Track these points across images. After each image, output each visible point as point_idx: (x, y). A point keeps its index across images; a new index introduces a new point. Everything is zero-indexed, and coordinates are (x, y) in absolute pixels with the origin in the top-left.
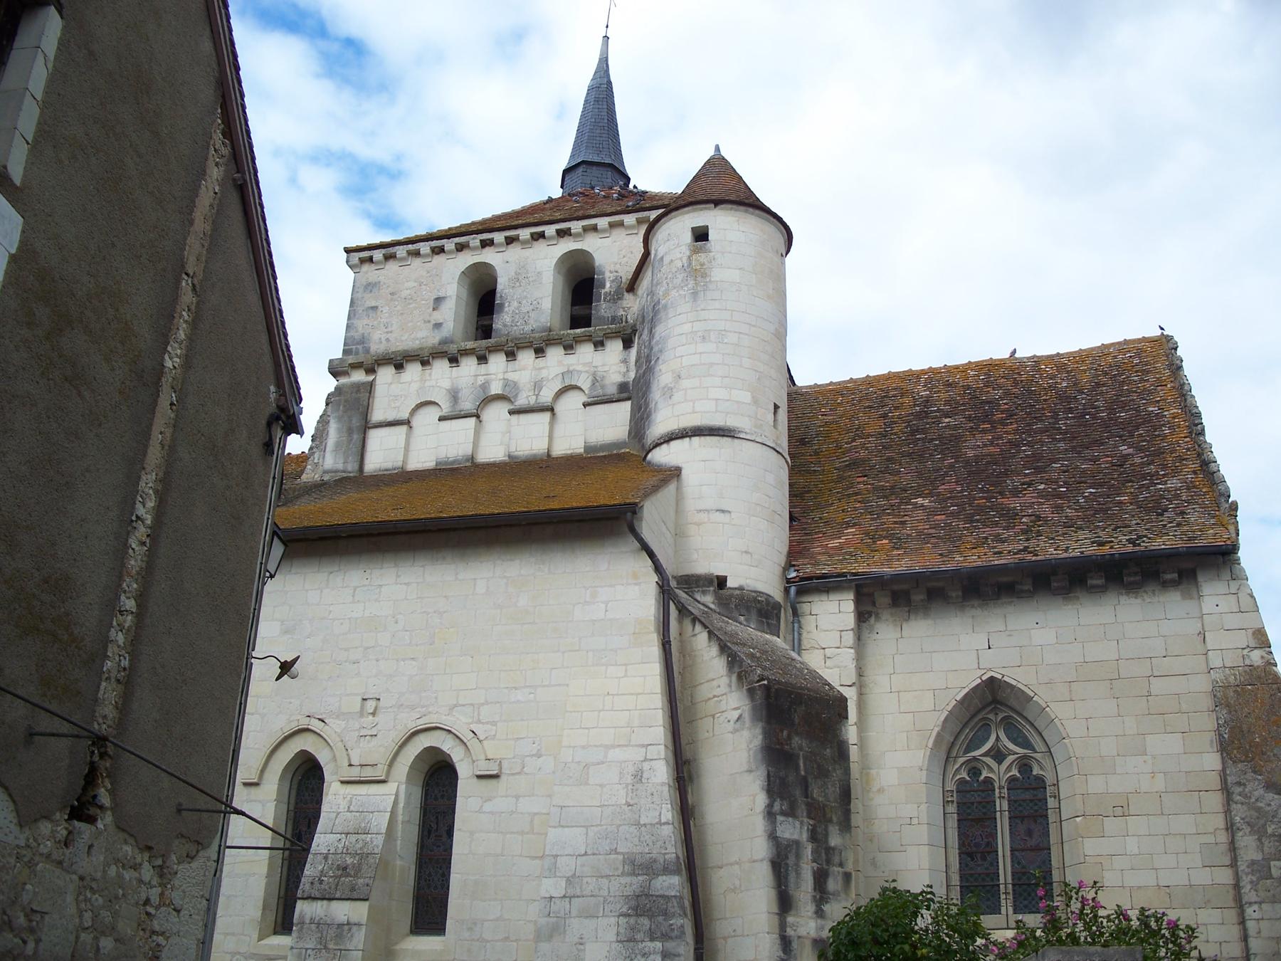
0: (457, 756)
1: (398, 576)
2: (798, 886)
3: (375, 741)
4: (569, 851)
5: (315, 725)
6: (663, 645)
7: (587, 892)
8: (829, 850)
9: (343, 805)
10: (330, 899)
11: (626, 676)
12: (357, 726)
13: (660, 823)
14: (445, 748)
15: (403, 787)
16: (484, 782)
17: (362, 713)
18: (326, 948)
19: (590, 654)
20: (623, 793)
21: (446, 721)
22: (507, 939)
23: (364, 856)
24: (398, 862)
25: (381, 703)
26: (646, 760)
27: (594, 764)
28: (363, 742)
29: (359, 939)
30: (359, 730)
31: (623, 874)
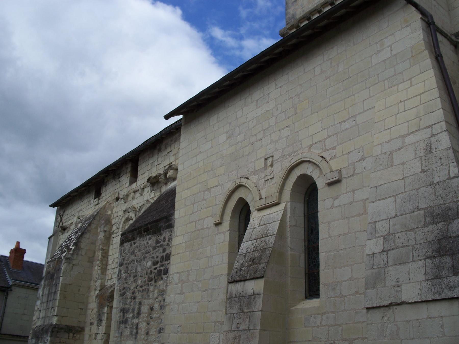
0: (315, 175)
1: (276, 85)
3: (273, 181)
4: (385, 216)
5: (244, 181)
6: (436, 58)
7: (399, 245)
9: (257, 223)
10: (245, 280)
11: (411, 86)
12: (264, 175)
13: (450, 178)
14: (308, 173)
15: (289, 204)
17: (265, 167)
18: (243, 312)
19: (386, 82)
20: (418, 164)
21: (306, 155)
22: (357, 293)
23: (263, 250)
24: (290, 252)
25: (275, 158)
26: (433, 135)
27: (396, 151)
28: (267, 184)
29: (259, 302)
30: (264, 178)
31: (425, 225)
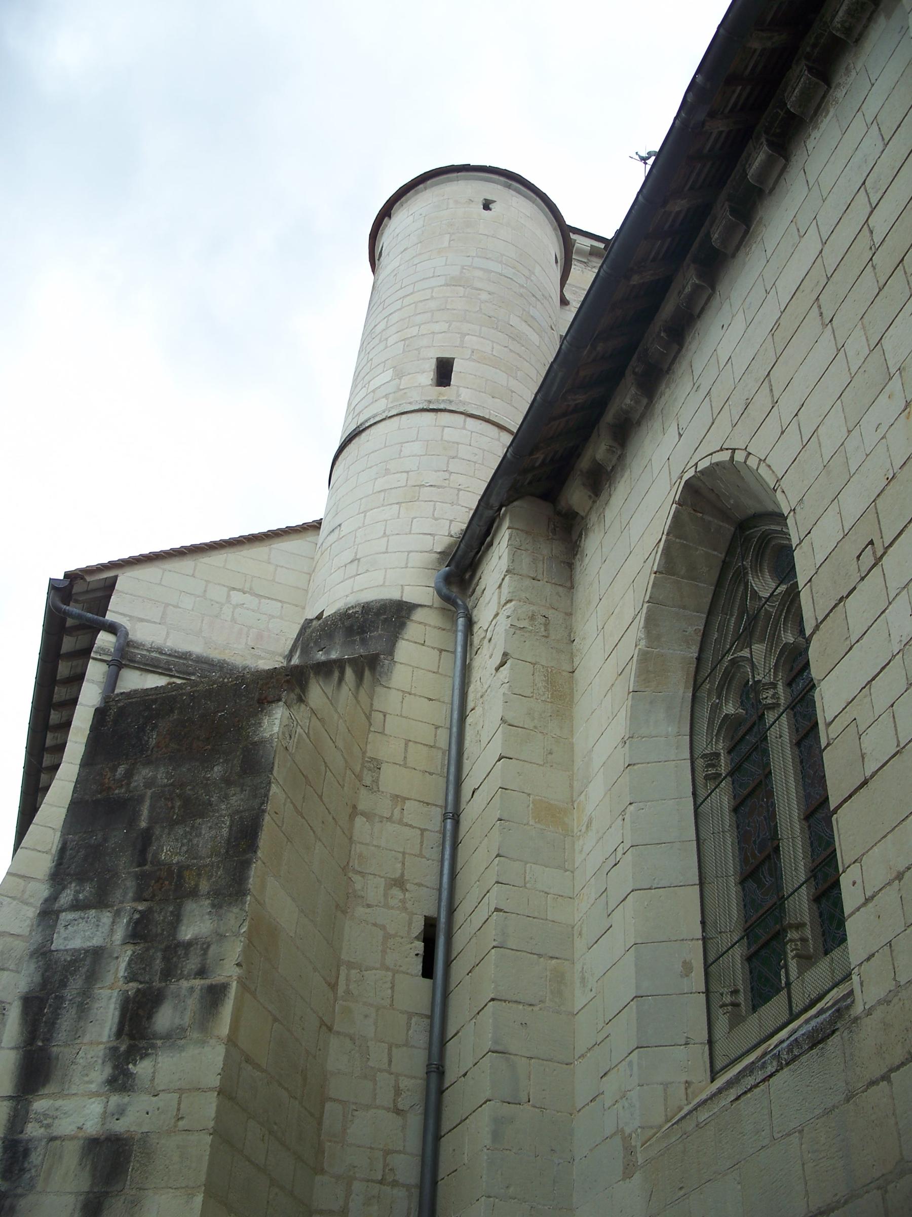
2: (76, 1033)
8: (175, 951)
16: (905, 468)
